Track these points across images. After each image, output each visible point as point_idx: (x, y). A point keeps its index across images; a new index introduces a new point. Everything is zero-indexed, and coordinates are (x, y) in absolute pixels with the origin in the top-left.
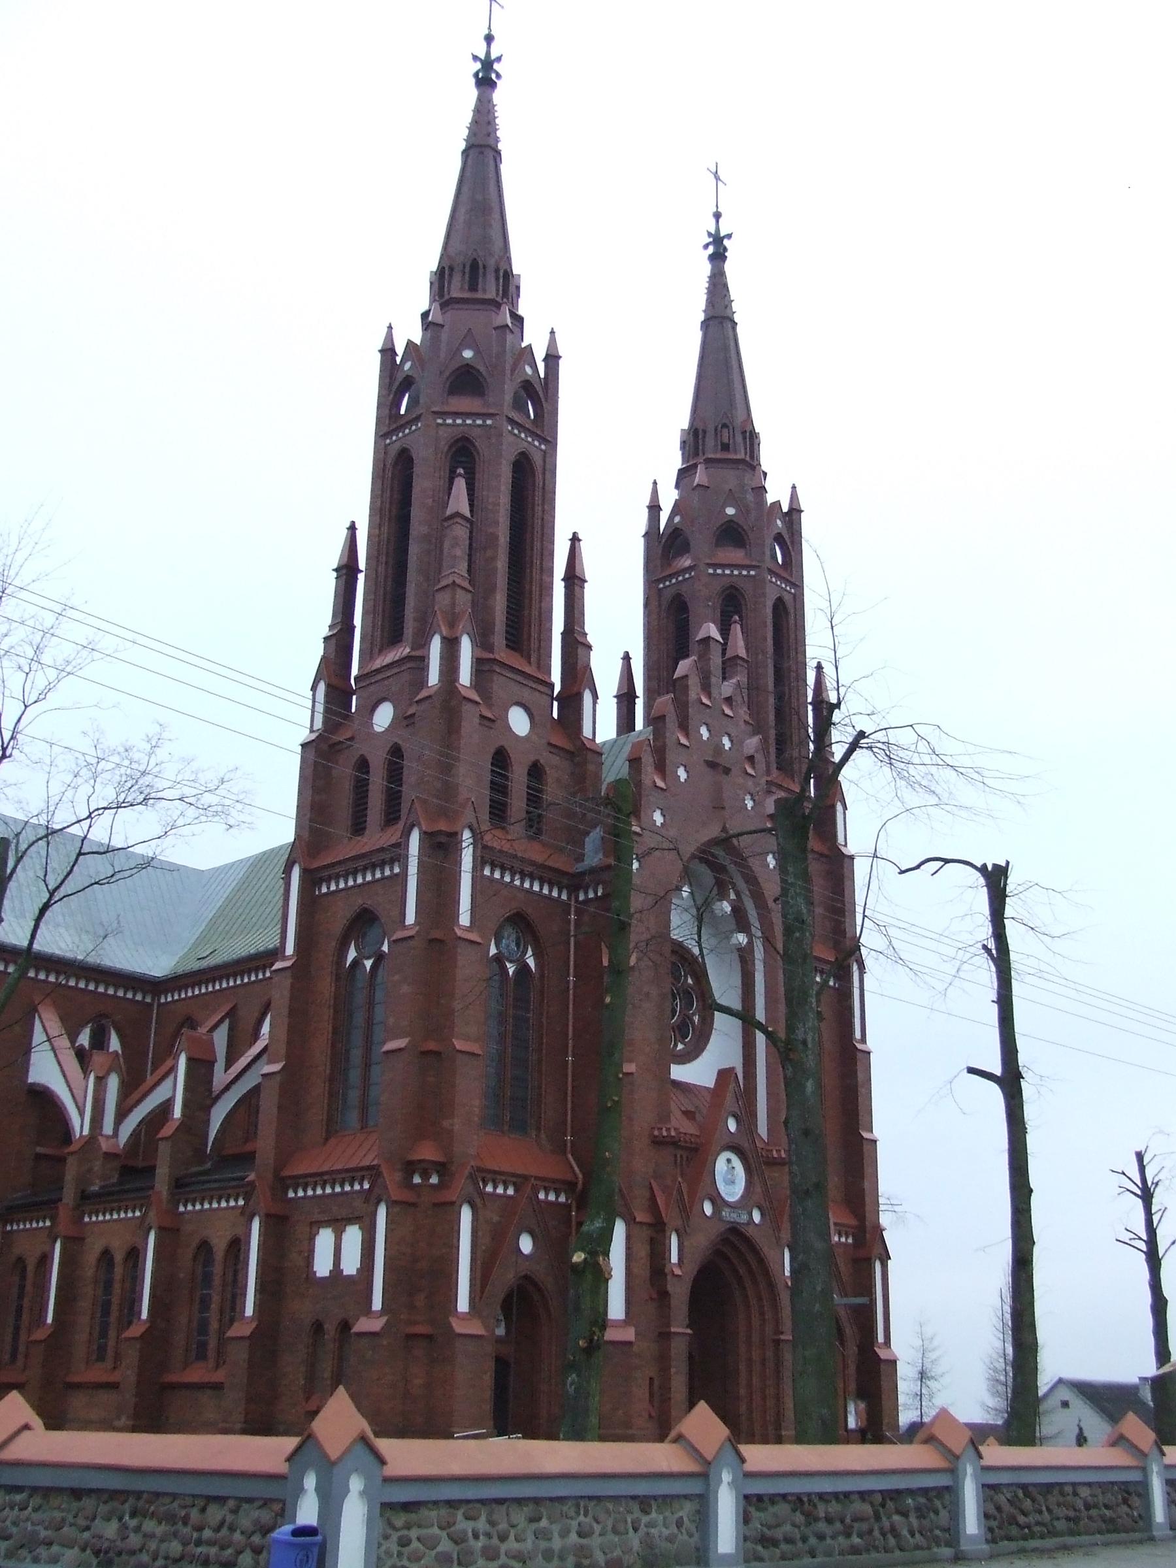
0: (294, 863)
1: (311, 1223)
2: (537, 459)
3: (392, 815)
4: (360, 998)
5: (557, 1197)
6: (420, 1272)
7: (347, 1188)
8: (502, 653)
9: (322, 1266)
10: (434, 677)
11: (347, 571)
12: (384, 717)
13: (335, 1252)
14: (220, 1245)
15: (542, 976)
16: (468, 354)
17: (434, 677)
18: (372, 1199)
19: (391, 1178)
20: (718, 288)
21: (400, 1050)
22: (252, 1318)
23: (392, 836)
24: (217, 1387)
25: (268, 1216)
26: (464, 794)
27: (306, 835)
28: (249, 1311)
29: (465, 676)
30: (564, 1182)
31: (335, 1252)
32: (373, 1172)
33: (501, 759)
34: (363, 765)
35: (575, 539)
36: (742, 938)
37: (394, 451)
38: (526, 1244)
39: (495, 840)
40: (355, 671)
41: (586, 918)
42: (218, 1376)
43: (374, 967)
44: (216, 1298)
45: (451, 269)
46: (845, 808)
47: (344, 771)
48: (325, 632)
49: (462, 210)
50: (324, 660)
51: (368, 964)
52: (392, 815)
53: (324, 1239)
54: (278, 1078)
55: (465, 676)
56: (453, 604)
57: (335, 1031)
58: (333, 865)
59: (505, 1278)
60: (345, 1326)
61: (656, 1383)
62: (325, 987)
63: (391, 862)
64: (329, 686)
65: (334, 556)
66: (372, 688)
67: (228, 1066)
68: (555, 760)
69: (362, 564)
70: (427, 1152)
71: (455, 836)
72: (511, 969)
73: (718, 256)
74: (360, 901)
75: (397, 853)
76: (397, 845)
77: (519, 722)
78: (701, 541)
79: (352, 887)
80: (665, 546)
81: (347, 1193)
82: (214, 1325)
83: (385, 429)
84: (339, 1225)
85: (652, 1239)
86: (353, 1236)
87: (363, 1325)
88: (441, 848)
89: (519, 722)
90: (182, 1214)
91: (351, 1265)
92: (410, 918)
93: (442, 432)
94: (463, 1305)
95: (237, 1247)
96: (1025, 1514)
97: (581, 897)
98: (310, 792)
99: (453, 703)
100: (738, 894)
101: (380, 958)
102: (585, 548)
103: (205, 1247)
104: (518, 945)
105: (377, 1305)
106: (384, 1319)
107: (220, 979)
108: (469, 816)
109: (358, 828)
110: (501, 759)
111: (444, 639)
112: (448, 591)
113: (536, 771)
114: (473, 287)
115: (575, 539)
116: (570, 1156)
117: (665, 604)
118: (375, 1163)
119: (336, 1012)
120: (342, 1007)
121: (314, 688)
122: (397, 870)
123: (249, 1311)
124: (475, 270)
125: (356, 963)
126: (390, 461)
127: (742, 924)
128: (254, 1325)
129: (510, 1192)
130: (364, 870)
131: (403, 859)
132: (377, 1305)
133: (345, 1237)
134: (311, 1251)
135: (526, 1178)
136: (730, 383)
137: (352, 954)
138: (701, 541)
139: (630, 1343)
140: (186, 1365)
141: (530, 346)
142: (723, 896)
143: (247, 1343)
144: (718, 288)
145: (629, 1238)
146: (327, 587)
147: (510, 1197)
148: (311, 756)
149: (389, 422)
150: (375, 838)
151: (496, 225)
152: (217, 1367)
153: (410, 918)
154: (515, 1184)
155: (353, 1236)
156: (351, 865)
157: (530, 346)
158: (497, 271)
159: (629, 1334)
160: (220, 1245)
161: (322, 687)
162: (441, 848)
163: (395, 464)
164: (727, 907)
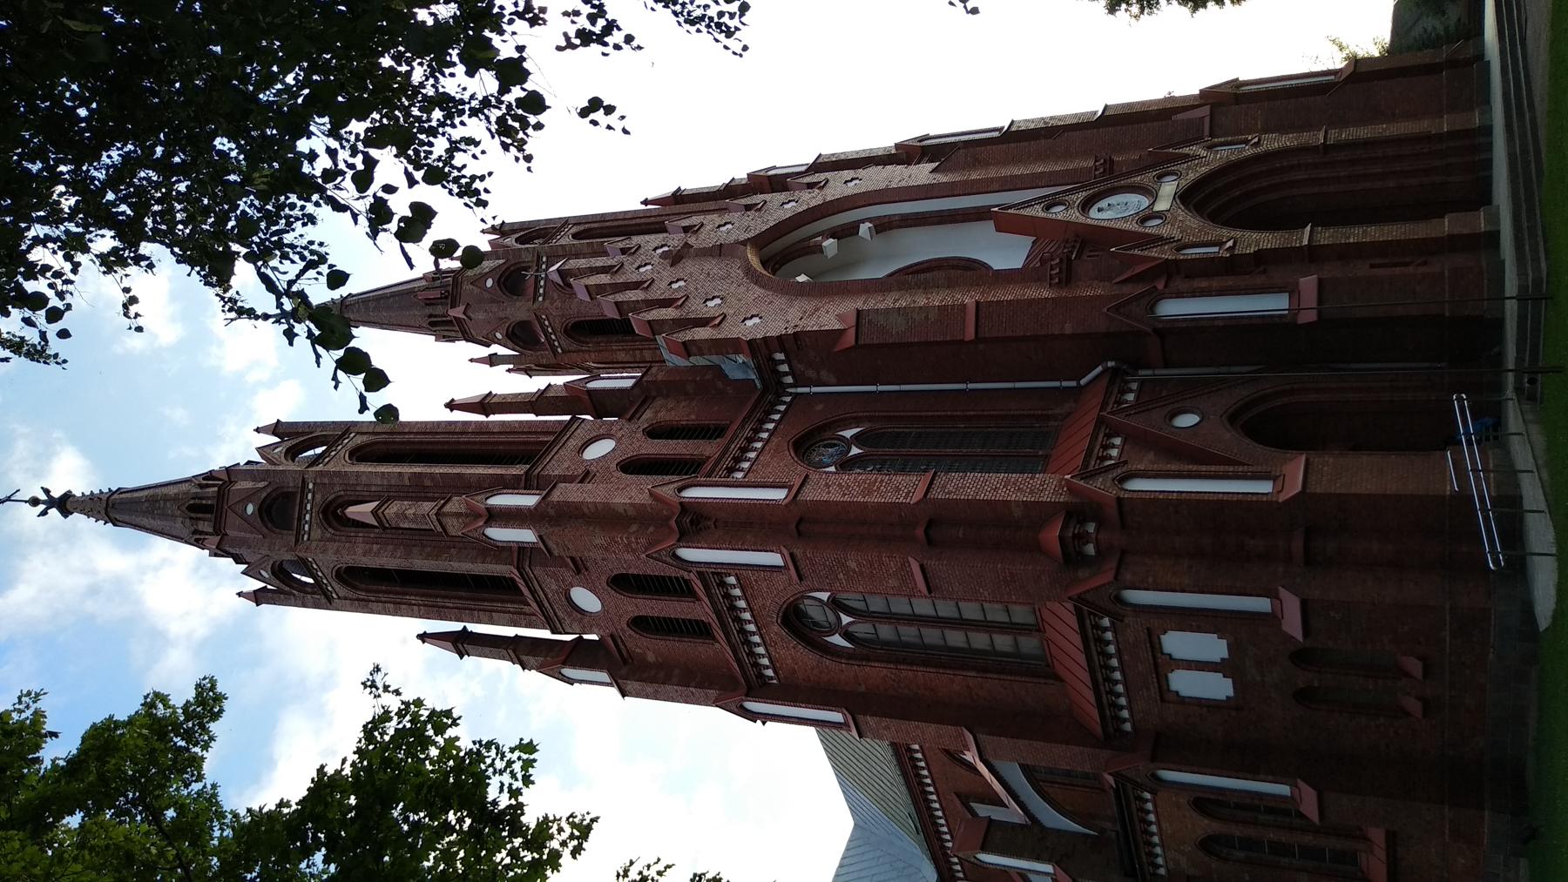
0: (742, 707)
1: (1163, 700)
2: (359, 440)
5: (1131, 391)
6: (1218, 543)
7: (1112, 649)
9: (1219, 687)
10: (527, 536)
11: (462, 644)
12: (586, 599)
13: (1198, 668)
14: (1206, 826)
15: (870, 419)
16: (250, 509)
17: (527, 536)
18: (1119, 610)
19: (1093, 581)
21: (922, 567)
22: (1294, 785)
24: (1391, 838)
25: (1153, 759)
26: (643, 498)
27: (713, 693)
28: (1284, 790)
30: (1111, 383)
31: (1198, 668)
32: (1086, 610)
33: (633, 466)
34: (641, 624)
35: (451, 405)
36: (864, 229)
38: (1187, 420)
40: (545, 634)
41: (811, 373)
42: (1377, 835)
44: (1272, 835)
45: (195, 532)
46: (927, 137)
47: (649, 648)
48: (98, 721)
49: (145, 521)
50: (541, 669)
51: (846, 619)
53: (1184, 683)
54: (981, 737)
55: (529, 501)
56: (458, 515)
57: (925, 664)
58: (739, 661)
59: (1228, 439)
60: (1301, 657)
61: (1378, 261)
62: (876, 673)
63: (723, 584)
64: (565, 663)
66: (560, 614)
67: (1003, 804)
68: (648, 414)
69: (456, 626)
70: (1052, 535)
71: (687, 507)
72: (855, 451)
74: (776, 628)
76: (701, 575)
77: (599, 450)
78: (519, 310)
79: (761, 637)
81: (1118, 650)
82: (1308, 839)
83: (324, 600)
84: (1163, 664)
85: (1187, 277)
86: (1176, 643)
87: (1293, 624)
88: (699, 523)
89: (599, 450)
90: (1168, 871)
91: (1213, 647)
92: (774, 559)
93: (317, 533)
94: (1265, 487)
95: (1205, 802)
97: (789, 380)
98: (669, 687)
99: (552, 512)
100: (818, 234)
101: (836, 604)
102: (460, 395)
103: (1208, 844)
104: (832, 446)
105: (1261, 604)
106: (1283, 593)
107: (933, 817)
108: (667, 492)
110: (633, 466)
111: (488, 523)
112: (444, 520)
113: (653, 433)
115: (451, 405)
116: (1083, 382)
117: (574, 347)
118: (1070, 606)
119: (904, 662)
120: (897, 653)
121: (571, 681)
122: (732, 580)
123: (1284, 790)
125: (847, 635)
126: (351, 594)
127: (851, 230)
128: (1301, 783)
129: (1118, 441)
131: (721, 570)
132: (1261, 604)
133: (1177, 654)
134: (1200, 702)
135: (1100, 422)
136: (393, 295)
137: (837, 640)
138: (519, 310)
139: (1320, 281)
141: (258, 449)
142: (819, 249)
145: (1179, 295)
147: (1124, 442)
148: (631, 685)
149: (319, 597)
151: (165, 490)
152: (1366, 839)
153: (774, 559)
154: (1109, 436)
155: (1176, 643)
157: (258, 449)
158: (201, 486)
160: (1206, 826)
161: (567, 672)
162: (699, 523)
163: (355, 588)
164: (829, 243)
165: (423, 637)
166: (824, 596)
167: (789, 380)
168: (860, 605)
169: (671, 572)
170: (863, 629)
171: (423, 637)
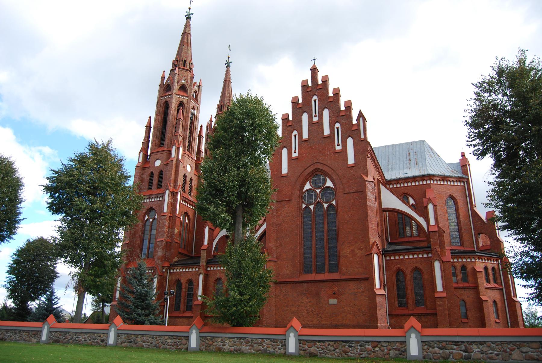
3: (159, 186)
4: (148, 228)
8: (186, 151)
11: (149, 127)
12: (158, 163)
20: (228, 74)
23: (159, 191)
29: (180, 157)
33: (185, 176)
34: (152, 174)
37: (163, 101)
39: (184, 195)
43: (153, 221)
46: (469, 166)
47: (146, 176)
48: (143, 141)
51: (151, 220)
52: (159, 186)
64: (144, 154)
65: (146, 123)
69: (152, 126)
71: (177, 193)
73: (228, 67)
75: (163, 195)
80: (207, 127)
88: (174, 195)
96: (185, 345)
101: (154, 219)
109: (150, 188)
110: (185, 176)
113: (191, 179)
114: (184, 66)
118: (218, 229)
121: (139, 154)
124: (182, 62)
125: (147, 220)
130: (189, 204)
137: (147, 217)
140: (184, 312)
143: (200, 306)
144: (228, 74)
146: (143, 130)
150: (155, 190)
156: (189, 202)
159: (444, 295)
161: (142, 154)
162: (174, 195)
165: (150, 118)
166: (156, 217)
167: (172, 271)
168: (153, 224)
169: (167, 141)
170: (148, 223)
171: (150, 118)
